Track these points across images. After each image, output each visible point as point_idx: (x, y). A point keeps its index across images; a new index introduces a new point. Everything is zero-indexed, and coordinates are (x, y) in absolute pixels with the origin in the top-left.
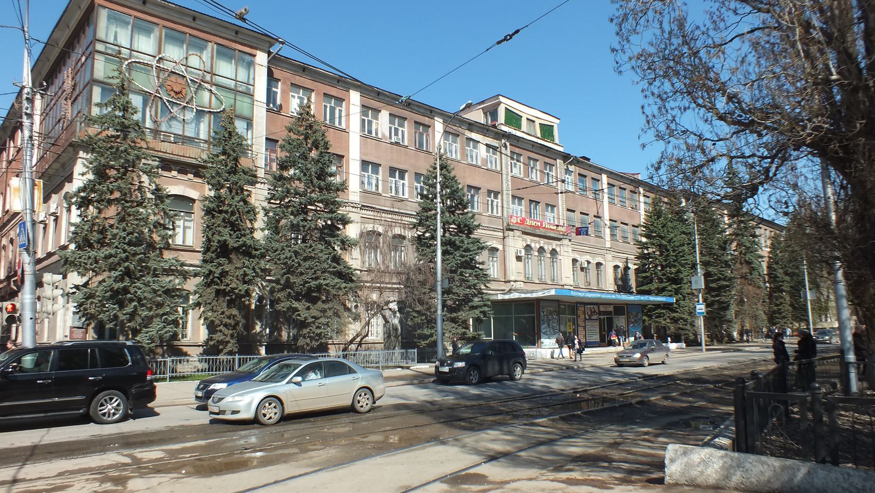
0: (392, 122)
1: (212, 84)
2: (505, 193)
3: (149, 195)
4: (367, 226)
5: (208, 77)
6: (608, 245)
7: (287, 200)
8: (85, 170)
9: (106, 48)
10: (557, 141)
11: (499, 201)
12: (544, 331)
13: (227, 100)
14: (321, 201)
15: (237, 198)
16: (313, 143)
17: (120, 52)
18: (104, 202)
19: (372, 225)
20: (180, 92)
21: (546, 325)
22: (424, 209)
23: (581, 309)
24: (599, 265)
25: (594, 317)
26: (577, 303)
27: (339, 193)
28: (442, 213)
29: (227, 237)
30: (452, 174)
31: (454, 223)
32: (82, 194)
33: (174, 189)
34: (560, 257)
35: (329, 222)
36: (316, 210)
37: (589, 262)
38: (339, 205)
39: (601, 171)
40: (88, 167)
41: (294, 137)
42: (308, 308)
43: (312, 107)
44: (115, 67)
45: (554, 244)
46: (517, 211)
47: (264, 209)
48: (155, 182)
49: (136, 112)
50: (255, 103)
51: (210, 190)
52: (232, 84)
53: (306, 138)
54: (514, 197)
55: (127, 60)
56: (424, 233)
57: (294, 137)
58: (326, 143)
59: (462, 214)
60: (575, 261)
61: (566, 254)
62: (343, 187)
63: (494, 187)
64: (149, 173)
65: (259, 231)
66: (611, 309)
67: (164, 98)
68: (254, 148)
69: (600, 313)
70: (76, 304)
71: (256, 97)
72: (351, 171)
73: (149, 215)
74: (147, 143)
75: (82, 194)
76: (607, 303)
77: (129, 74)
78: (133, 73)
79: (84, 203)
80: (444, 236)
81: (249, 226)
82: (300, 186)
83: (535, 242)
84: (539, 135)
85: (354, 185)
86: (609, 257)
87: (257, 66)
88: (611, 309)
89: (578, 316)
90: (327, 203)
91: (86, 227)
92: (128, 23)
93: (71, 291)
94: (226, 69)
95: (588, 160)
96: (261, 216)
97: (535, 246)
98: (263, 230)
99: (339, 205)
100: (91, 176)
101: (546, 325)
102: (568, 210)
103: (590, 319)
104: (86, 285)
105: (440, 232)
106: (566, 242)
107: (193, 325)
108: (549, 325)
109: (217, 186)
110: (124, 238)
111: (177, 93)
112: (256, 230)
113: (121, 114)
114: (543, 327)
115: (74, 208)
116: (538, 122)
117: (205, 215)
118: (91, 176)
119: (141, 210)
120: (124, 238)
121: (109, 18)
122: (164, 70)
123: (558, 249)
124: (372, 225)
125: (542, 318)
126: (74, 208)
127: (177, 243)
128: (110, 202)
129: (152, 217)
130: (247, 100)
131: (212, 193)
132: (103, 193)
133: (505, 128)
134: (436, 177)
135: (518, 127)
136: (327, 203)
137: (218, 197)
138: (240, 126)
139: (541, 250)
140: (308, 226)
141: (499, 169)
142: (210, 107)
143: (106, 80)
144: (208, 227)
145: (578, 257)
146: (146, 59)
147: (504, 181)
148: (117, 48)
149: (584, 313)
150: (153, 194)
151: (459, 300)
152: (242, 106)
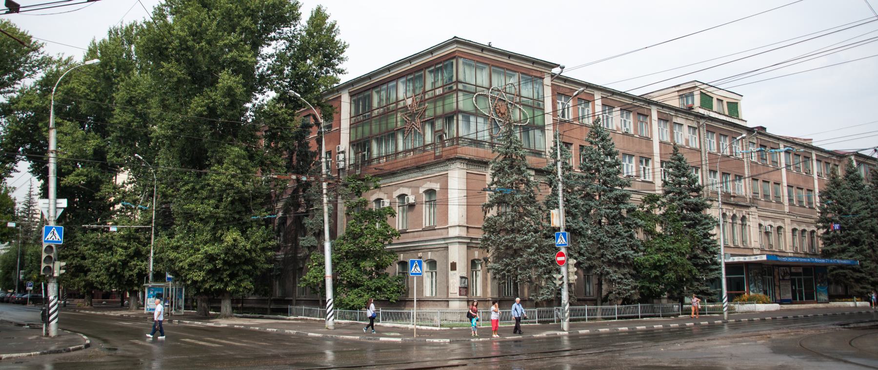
0: (622, 115)
2: (704, 167)
6: (787, 209)
10: (715, 109)
23: (776, 270)
24: (779, 228)
25: (787, 277)
26: (773, 265)
37: (771, 226)
39: (779, 139)
42: (615, 272)
45: (744, 211)
54: (710, 171)
60: (760, 225)
63: (776, 180)
66: (801, 270)
67: (496, 119)
69: (792, 274)
84: (727, 113)
86: (787, 221)
88: (801, 270)
89: (774, 277)
94: (527, 91)
95: (764, 129)
97: (729, 214)
103: (783, 279)
106: (753, 209)
116: (725, 101)
121: (464, 63)
123: (747, 216)
133: (702, 111)
135: (710, 108)
141: (698, 147)
145: (762, 222)
149: (778, 274)
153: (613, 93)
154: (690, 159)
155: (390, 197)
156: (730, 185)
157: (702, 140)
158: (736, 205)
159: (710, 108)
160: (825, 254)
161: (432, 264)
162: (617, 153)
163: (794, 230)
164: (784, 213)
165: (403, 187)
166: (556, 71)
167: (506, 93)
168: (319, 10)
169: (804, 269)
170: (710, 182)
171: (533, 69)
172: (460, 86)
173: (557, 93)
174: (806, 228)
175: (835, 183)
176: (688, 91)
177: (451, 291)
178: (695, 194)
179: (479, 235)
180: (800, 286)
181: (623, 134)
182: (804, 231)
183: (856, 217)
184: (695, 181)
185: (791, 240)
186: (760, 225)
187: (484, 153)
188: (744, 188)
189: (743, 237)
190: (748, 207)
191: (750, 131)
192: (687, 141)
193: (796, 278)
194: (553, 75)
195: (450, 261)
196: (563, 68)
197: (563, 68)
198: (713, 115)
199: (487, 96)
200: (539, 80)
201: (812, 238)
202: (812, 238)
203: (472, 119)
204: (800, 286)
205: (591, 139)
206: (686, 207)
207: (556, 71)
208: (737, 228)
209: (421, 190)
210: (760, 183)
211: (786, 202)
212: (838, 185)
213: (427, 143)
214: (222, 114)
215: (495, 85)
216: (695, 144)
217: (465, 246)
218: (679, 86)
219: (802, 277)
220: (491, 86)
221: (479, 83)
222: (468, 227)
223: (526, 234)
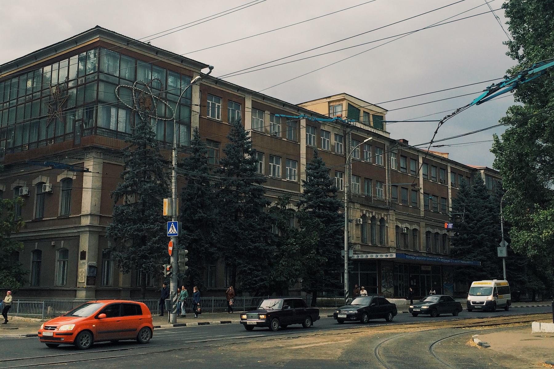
1: (166, 100)
6: (422, 214)
10: (362, 119)
12: (383, 285)
24: (415, 230)
60: (397, 227)
61: (391, 221)
66: (430, 269)
83: (369, 212)
84: (372, 124)
86: (423, 224)
88: (430, 269)
108: (386, 280)
114: (383, 281)
123: (385, 218)
141: (343, 153)
153: (264, 97)
154: (328, 163)
155: (29, 185)
156: (372, 190)
158: (376, 208)
159: (358, 120)
160: (454, 254)
161: (65, 252)
162: (328, 171)
163: (428, 233)
164: (419, 217)
165: (42, 175)
166: (205, 71)
168: (491, 151)
170: (346, 184)
171: (184, 67)
172: (102, 77)
173: (206, 92)
174: (439, 232)
175: (464, 192)
176: (338, 103)
177: (79, 280)
178: (331, 194)
179: (109, 224)
181: (271, 137)
184: (331, 183)
185: (425, 241)
186: (397, 227)
187: (121, 144)
188: (384, 193)
190: (387, 210)
191: (393, 142)
192: (333, 147)
194: (202, 75)
195: (81, 250)
196: (211, 68)
197: (211, 68)
198: (358, 125)
199: (131, 89)
200: (187, 79)
201: (444, 241)
202: (444, 241)
203: (113, 111)
205: (230, 136)
206: (324, 205)
207: (205, 71)
208: (377, 229)
209: (59, 179)
210: (399, 189)
211: (422, 209)
212: (467, 195)
213: (67, 132)
215: (141, 77)
216: (340, 151)
217: (97, 236)
218: (330, 97)
220: (136, 79)
221: (123, 75)
222: (101, 216)
223: (152, 223)
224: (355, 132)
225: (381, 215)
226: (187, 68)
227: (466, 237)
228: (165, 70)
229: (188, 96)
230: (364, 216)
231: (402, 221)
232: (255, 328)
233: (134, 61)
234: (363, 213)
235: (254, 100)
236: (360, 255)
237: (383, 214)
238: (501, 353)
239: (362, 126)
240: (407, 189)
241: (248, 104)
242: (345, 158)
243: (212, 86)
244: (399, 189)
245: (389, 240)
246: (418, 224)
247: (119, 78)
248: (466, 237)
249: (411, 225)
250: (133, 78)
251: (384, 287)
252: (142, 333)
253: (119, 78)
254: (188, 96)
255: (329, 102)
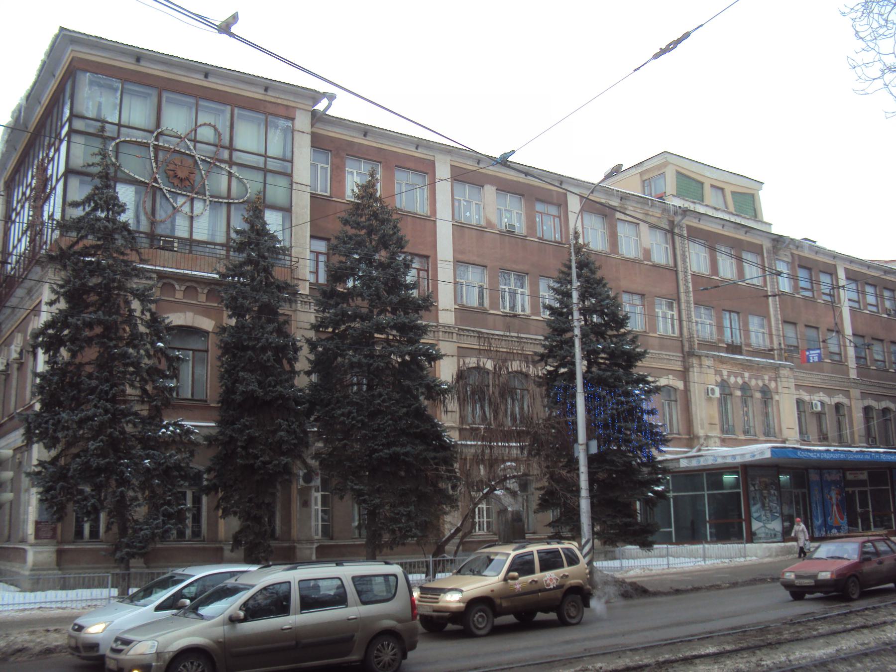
1: (231, 163)
3: (142, 329)
4: (467, 360)
5: (225, 155)
7: (343, 327)
8: (54, 297)
9: (87, 126)
11: (675, 313)
12: (755, 515)
13: (253, 184)
14: (394, 327)
15: (270, 327)
16: (380, 239)
17: (103, 129)
18: (77, 343)
19: (474, 360)
20: (188, 179)
21: (758, 506)
22: (555, 330)
24: (838, 407)
27: (422, 313)
28: (584, 335)
29: (254, 387)
30: (598, 275)
31: (603, 351)
32: (50, 331)
33: (176, 319)
34: (776, 397)
35: (407, 358)
36: (387, 341)
38: (424, 330)
40: (57, 293)
41: (351, 231)
43: (379, 186)
44: (96, 151)
46: (703, 325)
47: (309, 341)
48: (149, 310)
49: (124, 211)
50: (295, 186)
51: (230, 317)
52: (259, 161)
53: (369, 234)
55: (114, 139)
56: (557, 367)
57: (351, 231)
58: (400, 240)
59: (615, 336)
60: (799, 402)
61: (786, 391)
62: (428, 304)
64: (143, 297)
65: (302, 374)
66: (864, 476)
68: (294, 252)
70: (41, 489)
71: (296, 178)
72: (440, 277)
73: (141, 357)
74: (139, 254)
75: (50, 331)
76: (856, 466)
77: (117, 158)
78: (122, 157)
79: (52, 345)
80: (589, 370)
81: (287, 367)
82: (362, 305)
84: (732, 209)
85: (445, 299)
86: (855, 393)
87: (452, 260)
88: (864, 476)
90: (402, 328)
91: (56, 378)
92: (116, 90)
93: (37, 470)
95: (815, 242)
96: (305, 351)
98: (308, 373)
99: (423, 330)
100: (62, 305)
101: (758, 506)
102: (785, 322)
104: (55, 460)
105: (581, 366)
107: (208, 518)
108: (763, 506)
109: (238, 311)
110: (107, 393)
111: (181, 180)
112: (298, 373)
113: (103, 215)
114: (753, 509)
115: (40, 352)
116: (728, 190)
117: (223, 355)
118: (62, 305)
119: (131, 350)
120: (107, 393)
122: (164, 149)
123: (773, 385)
124: (474, 360)
125: (752, 495)
126: (40, 352)
127: (182, 396)
128: (89, 341)
129: (146, 361)
130: (283, 182)
131: (233, 322)
132: (77, 328)
134: (570, 282)
135: (701, 200)
136: (402, 328)
137: (239, 328)
138: (273, 221)
139: (745, 388)
140: (375, 365)
141: (671, 263)
142: (229, 197)
143: (84, 169)
144: (226, 371)
146: (139, 136)
147: (681, 283)
148: (99, 124)
150: (149, 327)
151: (616, 472)
152: (276, 191)
157: (678, 252)
159: (701, 200)
163: (867, 410)
167: (195, 141)
169: (870, 475)
171: (268, 102)
180: (864, 504)
182: (745, 388)
183: (796, 635)
189: (709, 430)
193: (857, 490)
204: (864, 504)
207: (321, 106)
214: (271, 333)
219: (868, 489)
224: (694, 223)
225: (763, 380)
226: (279, 101)
227: (600, 321)
228: (229, 108)
229: (289, 155)
230: (723, 385)
231: (812, 389)
232: (450, 627)
233: (154, 93)
234: (721, 375)
235: (454, 164)
236: (702, 459)
237: (766, 377)
238: (24, 434)
239: (710, 212)
240: (817, 328)
241: (443, 171)
242: (676, 272)
243: (356, 140)
244: (801, 328)
245: (784, 427)
246: (847, 394)
247: (119, 125)
248: (600, 321)
249: (830, 396)
250: (151, 126)
251: (758, 519)
252: (52, 628)
253: (119, 125)
254: (289, 155)
255: (641, 174)
